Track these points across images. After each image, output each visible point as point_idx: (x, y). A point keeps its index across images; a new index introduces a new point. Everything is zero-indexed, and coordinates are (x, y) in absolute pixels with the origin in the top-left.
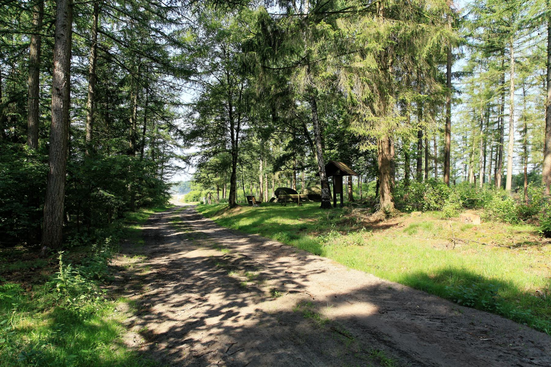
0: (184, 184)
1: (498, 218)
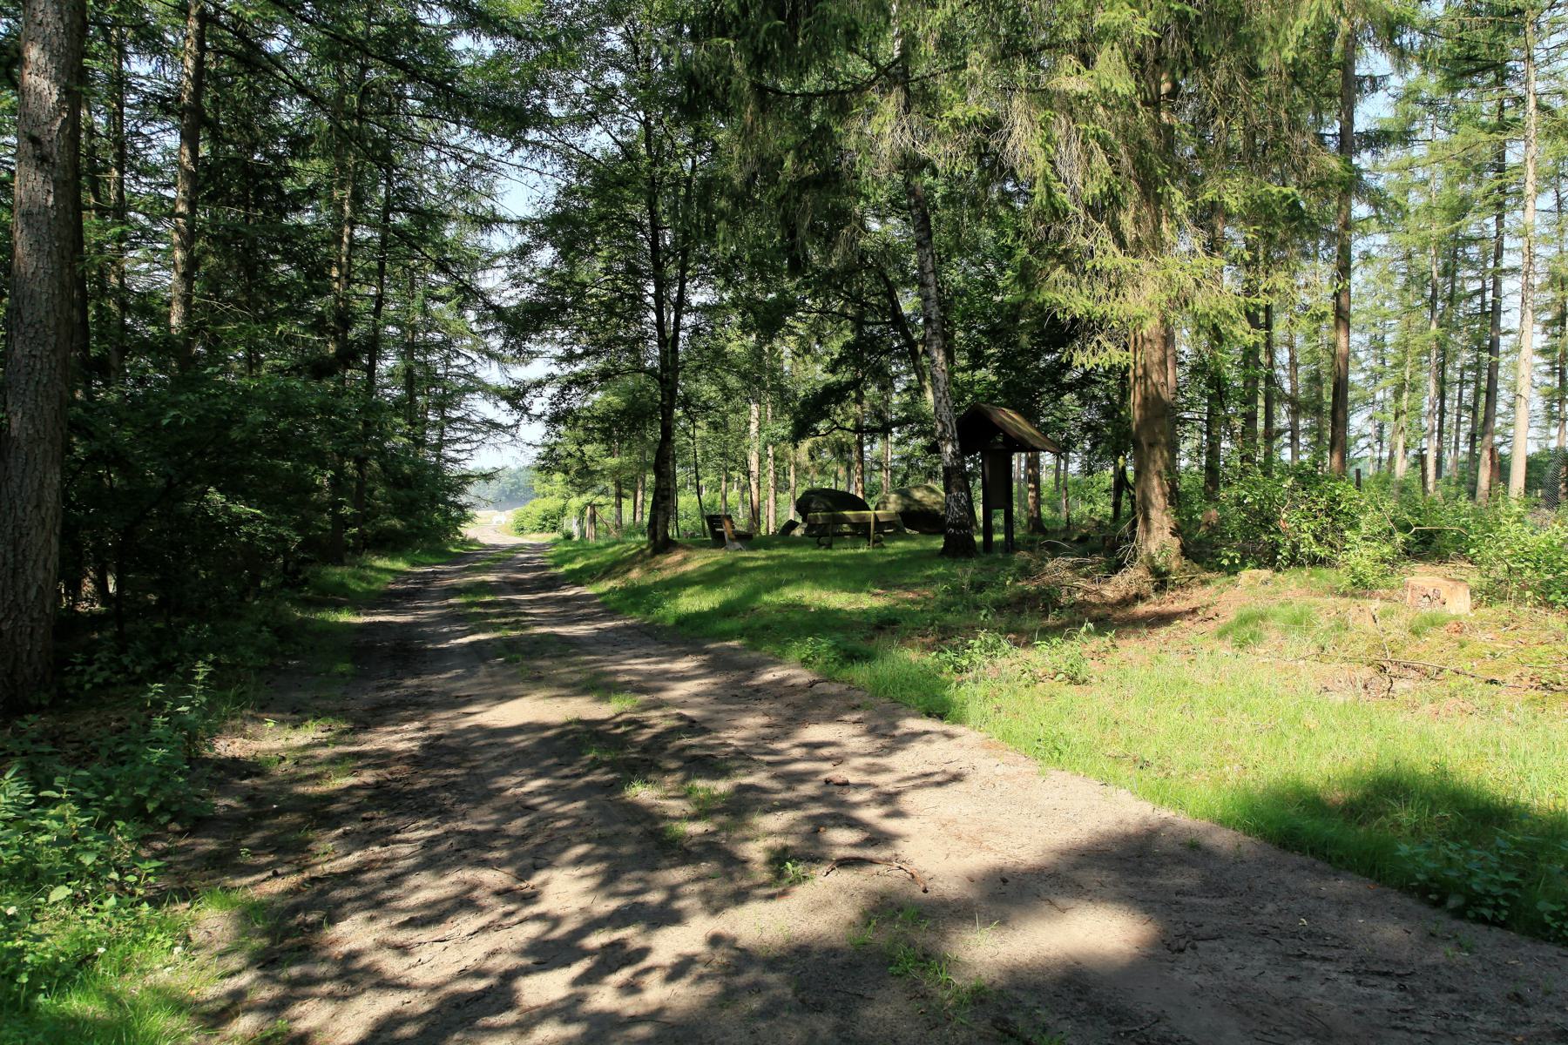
0: (509, 476)
1: (1528, 593)
